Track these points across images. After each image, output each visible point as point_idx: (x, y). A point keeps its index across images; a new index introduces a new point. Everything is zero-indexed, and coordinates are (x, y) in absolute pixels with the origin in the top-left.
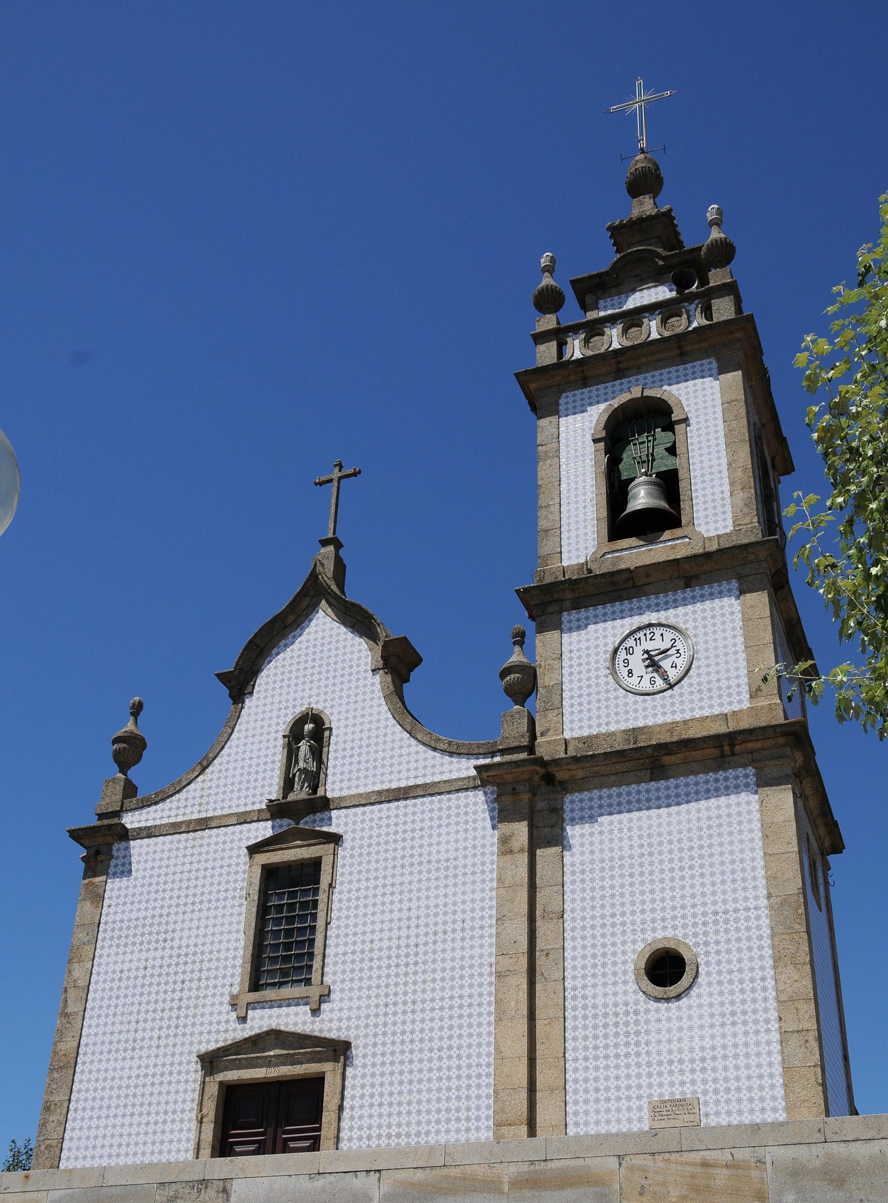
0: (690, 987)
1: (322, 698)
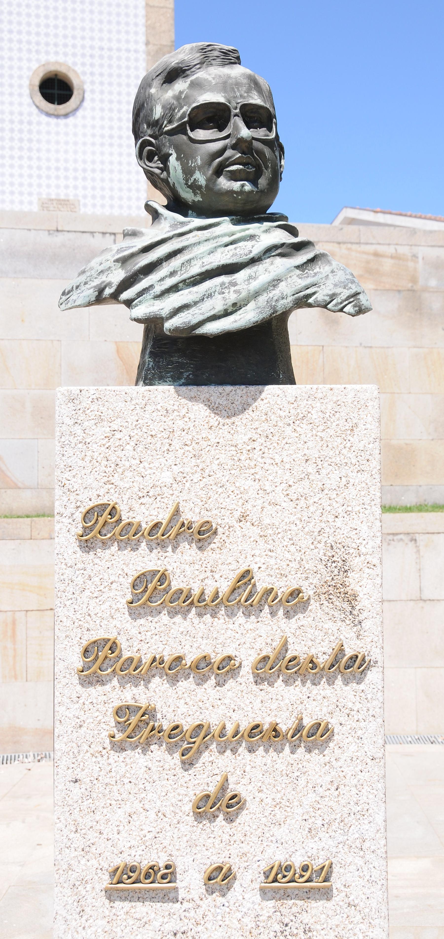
0: (76, 109)
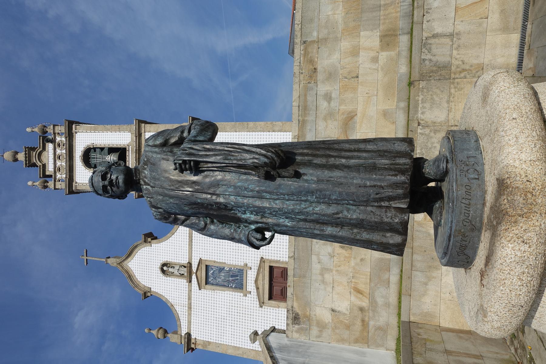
1: (157, 264)
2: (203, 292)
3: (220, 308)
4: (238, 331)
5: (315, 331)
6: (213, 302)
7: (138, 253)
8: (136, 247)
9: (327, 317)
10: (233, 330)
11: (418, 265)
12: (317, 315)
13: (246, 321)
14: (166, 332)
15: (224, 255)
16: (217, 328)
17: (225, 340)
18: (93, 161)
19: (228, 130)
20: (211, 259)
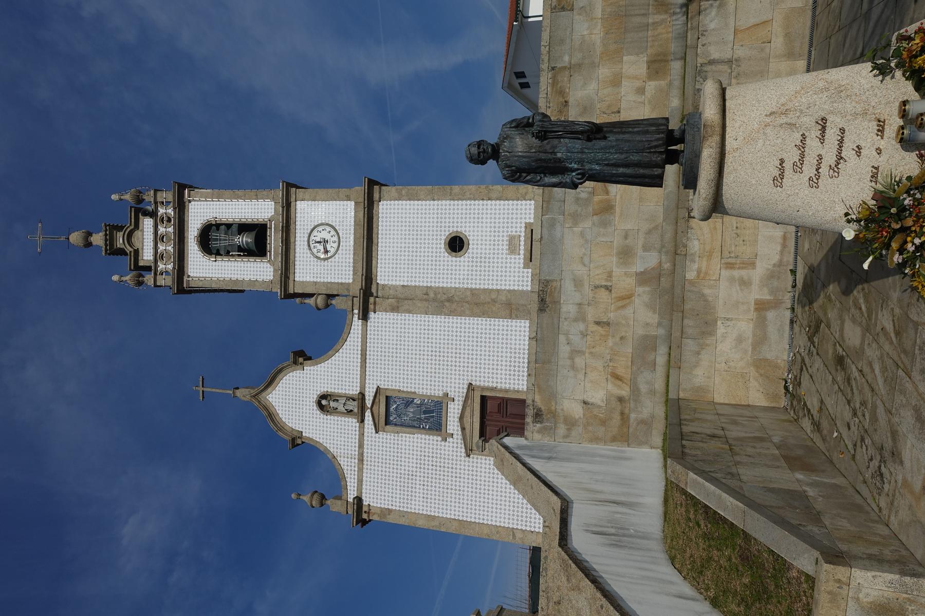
2: (381, 436)
3: (407, 460)
4: (433, 493)
5: (562, 430)
6: (396, 450)
7: (284, 381)
8: (280, 371)
9: (577, 411)
10: (425, 492)
11: (689, 331)
12: (565, 409)
13: (446, 478)
14: (323, 497)
15: (413, 381)
16: (402, 488)
17: (413, 507)
18: (214, 245)
19: (422, 197)
20: (394, 388)
